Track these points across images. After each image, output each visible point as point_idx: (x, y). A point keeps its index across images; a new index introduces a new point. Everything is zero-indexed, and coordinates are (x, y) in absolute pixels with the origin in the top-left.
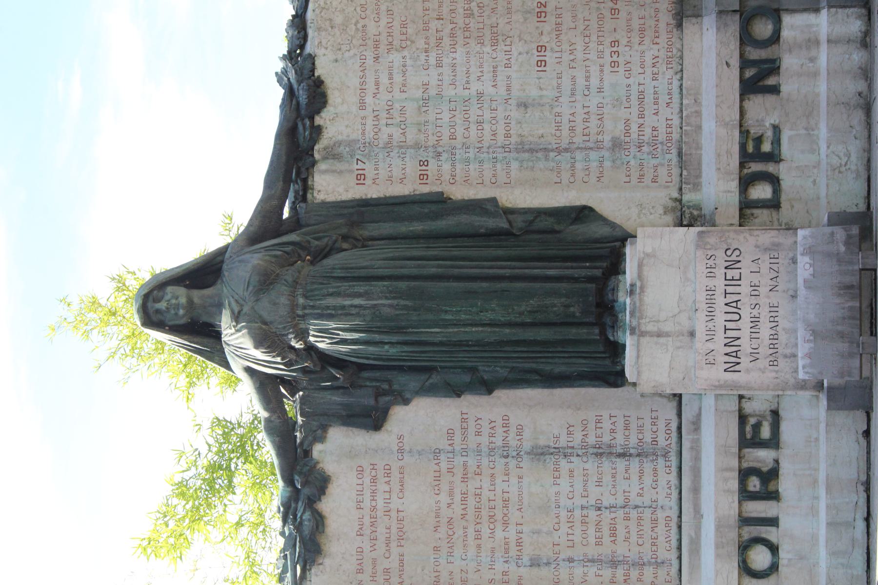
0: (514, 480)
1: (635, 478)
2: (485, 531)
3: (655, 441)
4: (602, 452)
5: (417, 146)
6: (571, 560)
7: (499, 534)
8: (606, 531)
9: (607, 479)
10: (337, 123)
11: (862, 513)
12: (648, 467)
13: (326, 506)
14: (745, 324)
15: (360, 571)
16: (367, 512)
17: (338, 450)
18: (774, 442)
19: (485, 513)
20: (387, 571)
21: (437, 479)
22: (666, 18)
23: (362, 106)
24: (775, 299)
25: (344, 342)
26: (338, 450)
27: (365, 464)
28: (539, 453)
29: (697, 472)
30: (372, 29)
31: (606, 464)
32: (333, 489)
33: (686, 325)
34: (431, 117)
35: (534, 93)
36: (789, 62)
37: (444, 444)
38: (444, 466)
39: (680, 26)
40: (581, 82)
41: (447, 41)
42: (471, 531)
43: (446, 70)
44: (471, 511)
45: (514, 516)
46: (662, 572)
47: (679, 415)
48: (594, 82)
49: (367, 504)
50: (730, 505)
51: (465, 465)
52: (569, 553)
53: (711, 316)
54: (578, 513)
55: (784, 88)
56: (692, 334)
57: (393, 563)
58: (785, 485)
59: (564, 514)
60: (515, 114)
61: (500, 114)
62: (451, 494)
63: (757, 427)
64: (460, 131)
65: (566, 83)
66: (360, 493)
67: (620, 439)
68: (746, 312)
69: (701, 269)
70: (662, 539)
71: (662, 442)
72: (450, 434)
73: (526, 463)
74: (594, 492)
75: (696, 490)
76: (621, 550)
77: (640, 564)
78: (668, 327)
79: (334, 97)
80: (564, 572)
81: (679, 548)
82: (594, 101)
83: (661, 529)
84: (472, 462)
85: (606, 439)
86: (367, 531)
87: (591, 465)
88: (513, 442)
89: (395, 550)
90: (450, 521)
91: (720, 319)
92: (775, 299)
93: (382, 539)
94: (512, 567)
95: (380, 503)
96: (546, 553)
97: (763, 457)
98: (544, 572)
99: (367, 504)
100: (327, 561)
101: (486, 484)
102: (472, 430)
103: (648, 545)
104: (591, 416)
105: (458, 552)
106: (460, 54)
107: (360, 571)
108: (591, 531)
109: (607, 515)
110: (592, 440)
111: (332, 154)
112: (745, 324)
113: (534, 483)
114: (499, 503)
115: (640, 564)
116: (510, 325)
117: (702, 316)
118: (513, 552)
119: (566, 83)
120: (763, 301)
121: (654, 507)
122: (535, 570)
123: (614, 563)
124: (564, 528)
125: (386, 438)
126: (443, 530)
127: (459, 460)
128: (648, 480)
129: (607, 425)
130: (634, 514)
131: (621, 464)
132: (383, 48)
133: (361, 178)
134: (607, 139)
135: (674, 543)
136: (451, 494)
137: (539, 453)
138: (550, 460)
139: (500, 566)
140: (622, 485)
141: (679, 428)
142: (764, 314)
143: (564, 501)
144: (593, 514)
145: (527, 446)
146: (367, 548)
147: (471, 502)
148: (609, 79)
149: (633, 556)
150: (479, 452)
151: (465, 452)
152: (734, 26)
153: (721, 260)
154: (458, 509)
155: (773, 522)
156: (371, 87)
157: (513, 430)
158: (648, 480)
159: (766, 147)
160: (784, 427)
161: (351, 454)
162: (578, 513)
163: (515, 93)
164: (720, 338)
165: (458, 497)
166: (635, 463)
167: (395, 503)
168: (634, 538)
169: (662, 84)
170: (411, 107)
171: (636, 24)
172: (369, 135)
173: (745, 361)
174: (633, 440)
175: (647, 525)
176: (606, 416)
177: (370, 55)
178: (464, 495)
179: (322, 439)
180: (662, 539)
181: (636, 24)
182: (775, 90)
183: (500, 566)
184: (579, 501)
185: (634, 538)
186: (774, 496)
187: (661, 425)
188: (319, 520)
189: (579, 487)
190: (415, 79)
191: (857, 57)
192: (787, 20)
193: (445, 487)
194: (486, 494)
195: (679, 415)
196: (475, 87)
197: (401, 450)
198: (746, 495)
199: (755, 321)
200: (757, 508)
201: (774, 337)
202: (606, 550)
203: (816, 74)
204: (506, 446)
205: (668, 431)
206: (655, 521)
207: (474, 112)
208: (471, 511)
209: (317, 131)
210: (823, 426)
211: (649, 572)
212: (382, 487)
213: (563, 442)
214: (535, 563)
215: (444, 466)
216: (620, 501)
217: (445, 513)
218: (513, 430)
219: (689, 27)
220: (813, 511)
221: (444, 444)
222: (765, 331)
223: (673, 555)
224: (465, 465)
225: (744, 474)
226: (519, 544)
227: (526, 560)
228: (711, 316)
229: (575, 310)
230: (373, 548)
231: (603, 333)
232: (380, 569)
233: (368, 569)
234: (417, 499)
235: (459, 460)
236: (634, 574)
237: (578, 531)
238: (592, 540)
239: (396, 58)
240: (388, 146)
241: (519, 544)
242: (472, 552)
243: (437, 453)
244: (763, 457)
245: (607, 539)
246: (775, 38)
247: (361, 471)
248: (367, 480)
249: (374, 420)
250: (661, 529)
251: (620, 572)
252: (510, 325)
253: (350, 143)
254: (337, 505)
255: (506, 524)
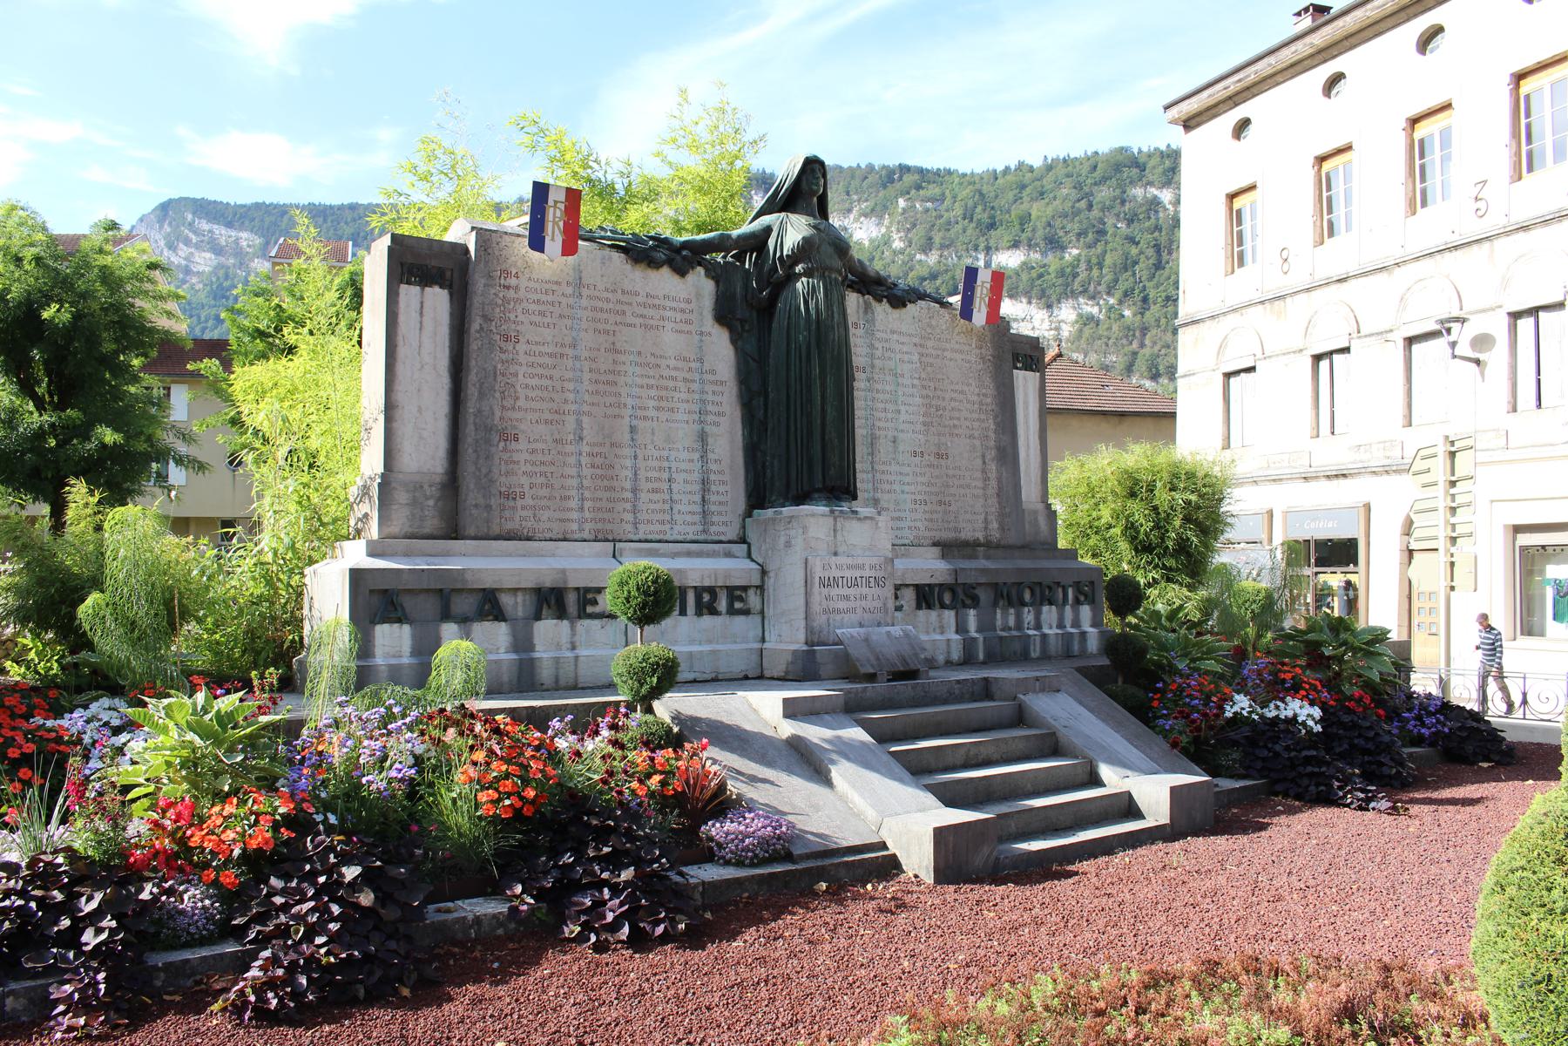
0: (686, 417)
1: (690, 508)
2: (653, 393)
3: (713, 524)
4: (704, 482)
5: (873, 366)
6: (636, 457)
7: (651, 403)
8: (656, 485)
9: (689, 488)
10: (882, 310)
11: (700, 677)
12: (697, 518)
13: (665, 271)
14: (845, 591)
15: (623, 292)
16: (662, 302)
17: (699, 287)
18: (732, 612)
19: (664, 393)
20: (624, 313)
21: (685, 359)
22: (938, 535)
23: (893, 332)
24: (859, 611)
25: (806, 302)
26: (699, 287)
27: (693, 306)
28: (703, 437)
29: (699, 554)
30: (930, 344)
31: (697, 487)
32: (676, 279)
33: (840, 550)
34: (888, 378)
35: (901, 448)
36: (933, 614)
37: (707, 366)
38: (693, 365)
39: (934, 544)
40: (907, 479)
41: (924, 392)
42: (652, 382)
43: (911, 390)
44: (664, 383)
45: (664, 416)
46: (629, 527)
47: (730, 542)
48: (906, 488)
49: (668, 304)
50: (693, 580)
51: (693, 381)
52: (640, 457)
53: (850, 567)
54: (666, 464)
55: (921, 613)
56: (836, 554)
57: (630, 319)
58: (707, 620)
59: (665, 453)
60: (890, 434)
61: (890, 425)
62: (676, 369)
63: (741, 599)
64: (881, 396)
65: (906, 470)
66: (674, 299)
67: (713, 498)
68: (852, 591)
69: (875, 561)
70: (652, 528)
71: (713, 529)
72: (713, 372)
73: (697, 427)
74: (680, 477)
75: (689, 554)
76: (644, 496)
77: (634, 511)
78: (839, 537)
79: (896, 313)
80: (627, 451)
81: (647, 541)
82: (896, 487)
83: (658, 527)
84: (695, 386)
85: (713, 488)
86: (650, 301)
87: (696, 476)
88: (710, 418)
89: (638, 321)
90: (658, 366)
91: (848, 574)
92: (859, 611)
93: (645, 312)
94: (630, 412)
95: (668, 314)
96: (640, 439)
97: (722, 605)
98: (627, 436)
99: (668, 304)
100: (629, 267)
101: (683, 396)
102: (716, 388)
103: (647, 517)
104: (726, 478)
105: (638, 370)
106: (918, 400)
107: (623, 292)
108: (656, 474)
109: (665, 486)
110: (712, 477)
111: (867, 307)
112: (845, 591)
113: (685, 434)
114: (671, 405)
115: (634, 511)
116: (823, 424)
117: (849, 561)
118: (640, 413)
119: (906, 470)
120: (858, 603)
121: (672, 522)
122: (628, 429)
123: (635, 491)
124: (656, 454)
125: (709, 324)
126: (653, 360)
127: (697, 377)
128: (689, 518)
129: (722, 489)
130: (667, 507)
131: (698, 498)
132: (920, 349)
133: (856, 325)
134: (878, 495)
135: (650, 537)
136: (676, 369)
137: (703, 437)
138: (698, 446)
139: (630, 402)
140: (685, 499)
141: (721, 542)
142: (851, 604)
143: (673, 454)
144: (666, 476)
145: (708, 428)
146: (640, 299)
147: (671, 384)
148: (909, 497)
149: (641, 506)
150: (702, 392)
151: (702, 382)
152: (949, 580)
153: (880, 574)
154: (666, 373)
155: (683, 612)
156: (902, 339)
157: (716, 419)
158: (689, 518)
159: (738, 605)
160: (742, 618)
161: (699, 296)
162: (666, 464)
163: (901, 435)
164: (838, 574)
165: (674, 373)
166: (698, 508)
167: (669, 325)
168: (652, 506)
169: (906, 533)
170: (891, 364)
171: (935, 516)
172: (879, 335)
173: (825, 591)
174: (713, 508)
175: (660, 517)
176: (728, 488)
177: (916, 340)
178: (674, 379)
179: (708, 275)
180: (652, 528)
181: (935, 516)
182: (919, 607)
183: (630, 402)
184: (674, 465)
185: (652, 506)
186: (699, 613)
187: (722, 529)
188: (654, 264)
189: (683, 466)
190: (906, 367)
191: (941, 658)
192: (952, 613)
193: (680, 364)
194: (677, 395)
195: (730, 542)
196: (903, 408)
197: (702, 333)
198: (699, 591)
199: (847, 598)
200: (691, 598)
201: (839, 611)
202: (644, 485)
203: (928, 633)
204: (707, 413)
205: (718, 534)
206: (663, 522)
207: (891, 407)
208: (664, 383)
209: (880, 301)
210: (744, 646)
211: (629, 517)
212: (679, 316)
213: (711, 456)
214: (633, 429)
215: (693, 365)
216: (675, 497)
217: (663, 362)
218: (716, 419)
219: (936, 551)
220: (692, 642)
221: (707, 366)
222: (842, 605)
223: (641, 536)
224: (693, 381)
225: (712, 590)
226: (645, 418)
227: (635, 422)
228: (850, 567)
229: (832, 472)
230: (639, 304)
231: (819, 491)
232: (625, 308)
233: (625, 298)
234: (671, 342)
235: (697, 377)
236: (628, 506)
237: (655, 464)
238: (649, 474)
239: (916, 358)
240: (872, 346)
241: (645, 418)
242: (639, 381)
243: (701, 360)
244: (722, 605)
245: (650, 486)
246: (943, 606)
247: (689, 301)
248: (683, 305)
249: (723, 315)
250: (658, 527)
251: (629, 495)
252: (823, 424)
253: (873, 320)
254: (663, 280)
255: (657, 409)
